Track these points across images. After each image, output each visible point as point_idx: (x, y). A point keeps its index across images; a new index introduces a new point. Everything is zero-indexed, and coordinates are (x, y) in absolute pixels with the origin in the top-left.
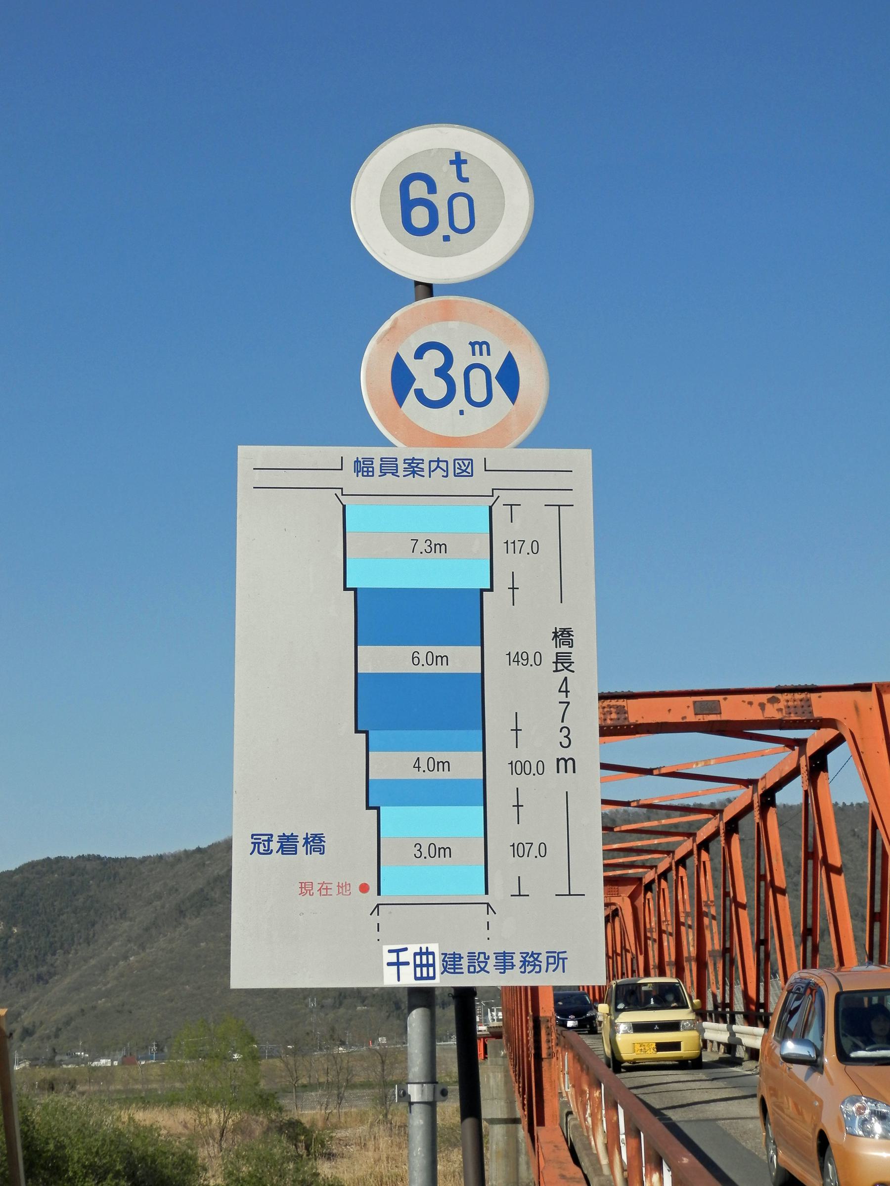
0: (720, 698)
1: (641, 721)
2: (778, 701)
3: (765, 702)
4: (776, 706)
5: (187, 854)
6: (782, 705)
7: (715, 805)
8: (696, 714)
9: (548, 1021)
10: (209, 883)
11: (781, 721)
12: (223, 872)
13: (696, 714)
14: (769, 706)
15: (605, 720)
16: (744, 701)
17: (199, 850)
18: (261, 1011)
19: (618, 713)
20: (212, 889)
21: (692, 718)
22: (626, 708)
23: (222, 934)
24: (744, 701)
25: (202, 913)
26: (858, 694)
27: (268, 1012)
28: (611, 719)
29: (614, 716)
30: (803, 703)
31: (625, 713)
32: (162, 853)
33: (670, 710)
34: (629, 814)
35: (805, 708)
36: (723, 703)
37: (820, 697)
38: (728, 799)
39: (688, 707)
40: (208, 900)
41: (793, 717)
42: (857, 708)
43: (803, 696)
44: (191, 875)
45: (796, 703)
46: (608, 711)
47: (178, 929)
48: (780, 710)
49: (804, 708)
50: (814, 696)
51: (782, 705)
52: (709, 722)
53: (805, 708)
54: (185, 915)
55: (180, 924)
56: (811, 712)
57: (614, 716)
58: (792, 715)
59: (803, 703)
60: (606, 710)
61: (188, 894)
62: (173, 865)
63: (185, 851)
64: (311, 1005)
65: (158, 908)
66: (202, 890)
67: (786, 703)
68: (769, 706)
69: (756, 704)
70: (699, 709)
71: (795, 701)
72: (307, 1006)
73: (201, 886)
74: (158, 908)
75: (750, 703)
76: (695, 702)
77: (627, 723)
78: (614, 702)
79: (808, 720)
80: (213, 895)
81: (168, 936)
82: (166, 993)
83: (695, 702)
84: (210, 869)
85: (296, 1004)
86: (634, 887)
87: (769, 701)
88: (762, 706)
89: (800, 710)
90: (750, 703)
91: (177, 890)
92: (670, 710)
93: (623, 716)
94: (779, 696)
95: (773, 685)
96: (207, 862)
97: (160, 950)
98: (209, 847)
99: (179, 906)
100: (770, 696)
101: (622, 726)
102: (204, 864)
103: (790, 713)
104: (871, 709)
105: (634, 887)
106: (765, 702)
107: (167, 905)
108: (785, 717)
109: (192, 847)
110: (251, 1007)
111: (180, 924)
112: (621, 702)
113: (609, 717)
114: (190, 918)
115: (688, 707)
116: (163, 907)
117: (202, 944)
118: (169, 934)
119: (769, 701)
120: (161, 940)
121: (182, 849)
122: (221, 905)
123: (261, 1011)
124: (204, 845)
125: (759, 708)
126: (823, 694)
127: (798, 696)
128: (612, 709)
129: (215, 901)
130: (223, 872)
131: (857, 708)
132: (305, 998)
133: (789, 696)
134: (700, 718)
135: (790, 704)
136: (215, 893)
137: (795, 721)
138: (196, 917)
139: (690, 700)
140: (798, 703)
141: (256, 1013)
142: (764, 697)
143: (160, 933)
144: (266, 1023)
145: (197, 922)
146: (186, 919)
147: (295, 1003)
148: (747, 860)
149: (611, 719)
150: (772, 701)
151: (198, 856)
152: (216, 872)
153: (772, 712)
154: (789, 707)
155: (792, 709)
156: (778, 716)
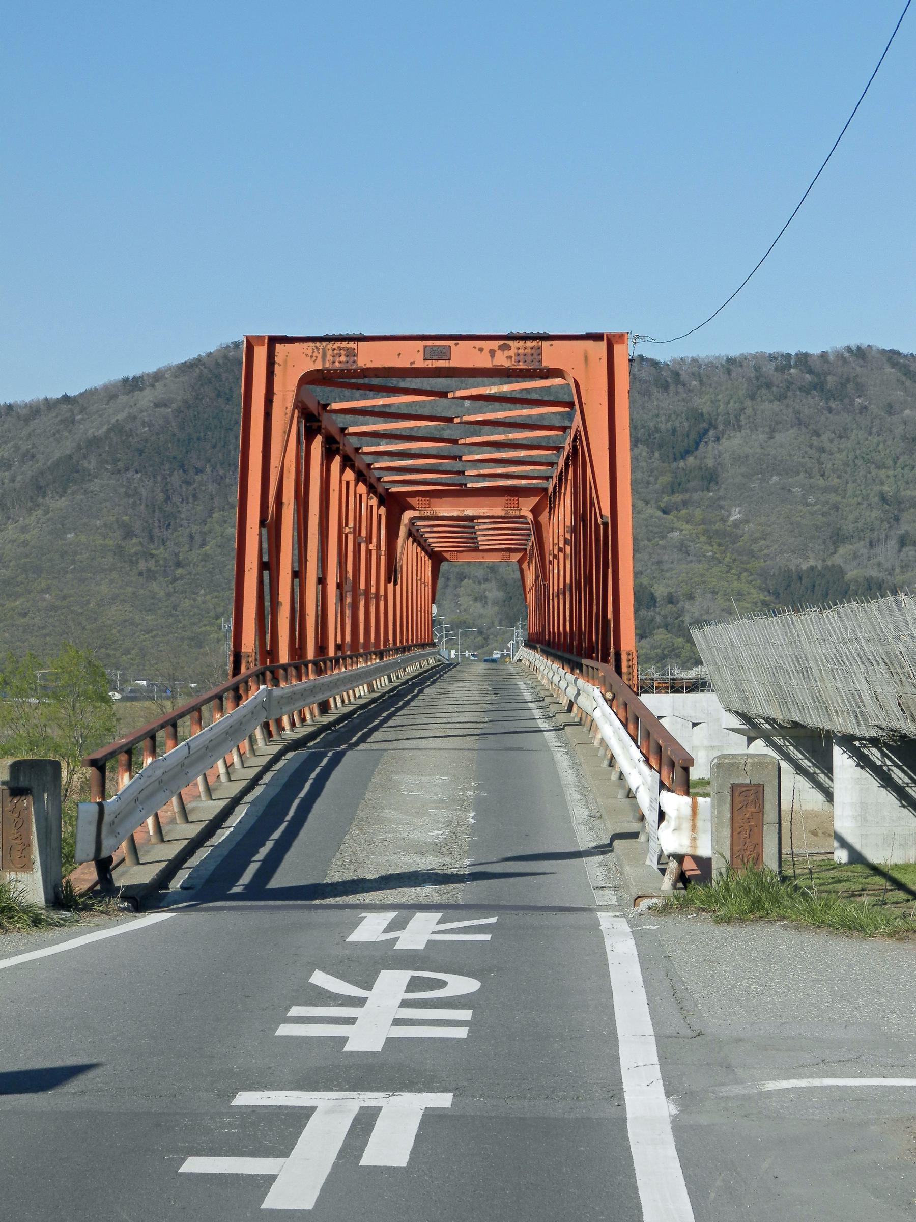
0: (451, 343)
1: (370, 365)
2: (509, 348)
3: (496, 349)
4: (507, 353)
5: (50, 405)
6: (512, 353)
7: (828, 356)
8: (425, 359)
9: (249, 656)
10: (79, 447)
11: (507, 369)
12: (100, 432)
13: (425, 359)
14: (499, 353)
15: (334, 362)
16: (475, 347)
17: (66, 399)
18: (154, 633)
19: (347, 356)
20: (85, 457)
21: (420, 364)
22: (356, 351)
23: (98, 522)
24: (475, 347)
25: (69, 492)
26: (590, 343)
27: (164, 636)
28: (340, 362)
29: (343, 359)
30: (533, 351)
31: (354, 356)
32: (12, 402)
33: (399, 355)
34: (700, 367)
35: (535, 356)
36: (453, 348)
37: (551, 345)
38: (848, 347)
39: (418, 351)
40: (78, 472)
41: (522, 366)
42: (586, 359)
43: (535, 343)
44: (54, 434)
45: (526, 351)
46: (337, 354)
47: (35, 513)
48: (510, 358)
49: (534, 357)
50: (545, 344)
51: (512, 353)
52: (436, 368)
53: (535, 356)
54: (45, 493)
55: (38, 506)
56: (540, 361)
57: (343, 359)
58: (521, 363)
59: (533, 351)
60: (336, 352)
61: (49, 463)
62: (27, 420)
63: (46, 399)
64: (225, 627)
65: (6, 481)
66: (70, 457)
67: (516, 351)
68: (499, 353)
69: (486, 351)
70: (430, 354)
71: (525, 348)
72: (220, 628)
73: (68, 452)
74: (6, 481)
75: (481, 350)
76: (425, 347)
77: (354, 367)
78: (344, 344)
79: (535, 370)
80: (86, 465)
81: (20, 522)
82: (18, 603)
83: (425, 347)
84: (82, 426)
85: (205, 625)
86: (538, 499)
87: (500, 348)
88: (492, 353)
89: (529, 358)
90: (481, 350)
91: (33, 456)
92: (399, 355)
93: (352, 359)
94: (510, 343)
95: (505, 332)
96: (78, 417)
97: (9, 542)
98: (82, 394)
99: (37, 480)
100: (501, 342)
101: (349, 370)
102: (73, 421)
103: (519, 361)
104: (600, 359)
105: (538, 499)
106: (496, 349)
107: (19, 478)
108: (514, 365)
109: (56, 394)
110: (139, 627)
111: (38, 506)
112: (351, 345)
113: (337, 359)
114: (53, 498)
115: (418, 351)
116: (13, 480)
117: (69, 536)
118: (21, 519)
119: (500, 348)
120: (10, 527)
121: (42, 397)
122: (96, 480)
123: (154, 633)
124: (73, 392)
125: (489, 355)
126: (555, 342)
127: (529, 344)
128: (342, 351)
129: (89, 475)
130: (100, 432)
131: (586, 359)
132: (217, 617)
133: (521, 343)
134: (429, 364)
135: (521, 351)
136: (89, 463)
137: (521, 370)
138: (61, 496)
139: (421, 344)
140: (528, 351)
141: (147, 636)
142: (495, 344)
143: (9, 518)
144: (161, 651)
145: (62, 503)
146: (47, 498)
147: (201, 624)
148: (869, 438)
149: (340, 362)
150: (503, 348)
151: (65, 407)
152: (90, 432)
153: (502, 360)
154: (519, 355)
155: (521, 357)
156: (507, 364)
